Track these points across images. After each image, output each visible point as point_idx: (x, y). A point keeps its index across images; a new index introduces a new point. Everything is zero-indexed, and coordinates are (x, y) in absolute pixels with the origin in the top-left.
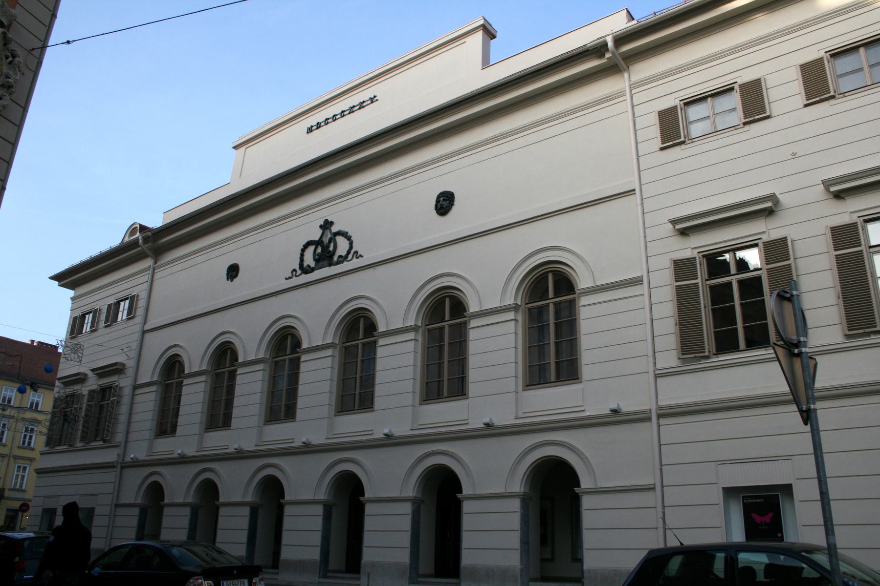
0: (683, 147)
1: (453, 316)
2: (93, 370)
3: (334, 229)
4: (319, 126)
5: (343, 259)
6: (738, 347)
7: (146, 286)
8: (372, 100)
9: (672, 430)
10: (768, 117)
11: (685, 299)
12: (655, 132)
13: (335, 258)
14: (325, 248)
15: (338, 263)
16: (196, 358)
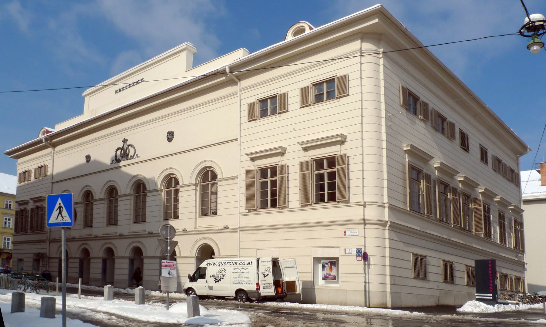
0: (310, 107)
1: (176, 186)
2: (31, 199)
3: (128, 143)
4: (120, 90)
5: (132, 157)
6: (324, 201)
7: (51, 161)
8: (142, 81)
9: (245, 236)
10: (348, 95)
11: (249, 186)
12: (246, 113)
13: (129, 156)
14: (125, 152)
15: (130, 159)
16: (99, 193)
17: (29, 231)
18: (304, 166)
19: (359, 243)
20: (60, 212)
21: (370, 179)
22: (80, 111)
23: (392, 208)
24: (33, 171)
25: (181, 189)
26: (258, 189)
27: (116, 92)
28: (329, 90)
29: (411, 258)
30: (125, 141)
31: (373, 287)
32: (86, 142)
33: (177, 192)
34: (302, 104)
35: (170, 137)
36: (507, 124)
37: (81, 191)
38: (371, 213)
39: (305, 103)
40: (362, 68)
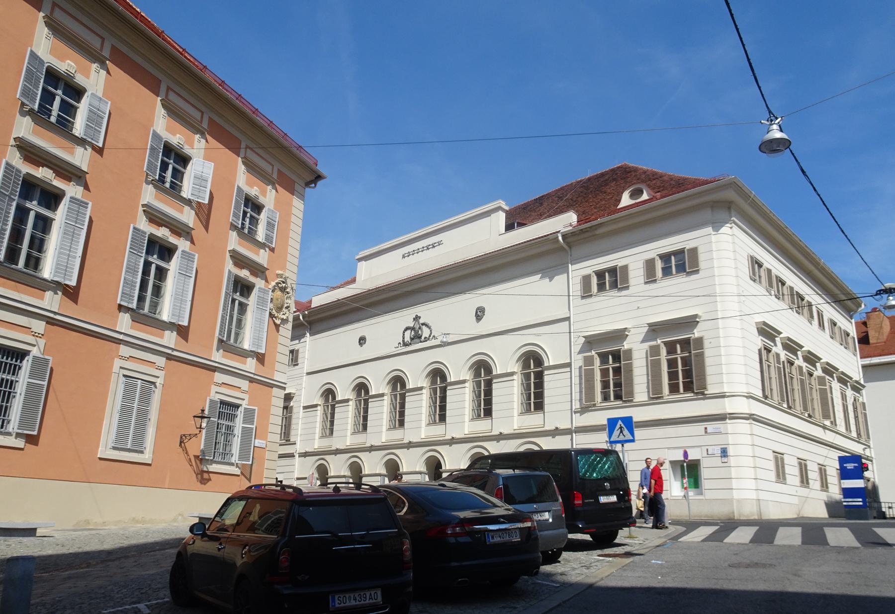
3: (421, 321)
5: (426, 339)
14: (416, 332)
20: (621, 432)
27: (404, 257)
29: (771, 456)
30: (417, 318)
36: (792, 229)
37: (520, 348)
39: (650, 277)
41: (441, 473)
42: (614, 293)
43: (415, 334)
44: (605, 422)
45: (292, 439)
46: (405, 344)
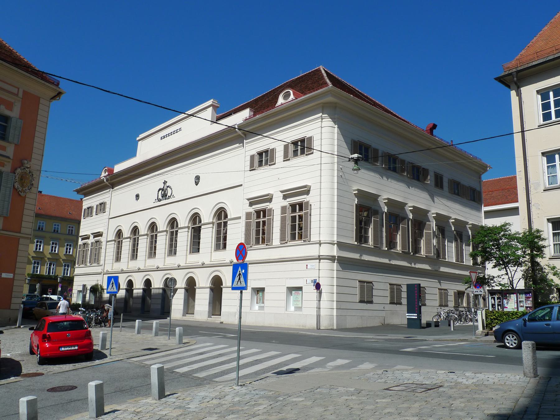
2: (92, 234)
3: (167, 185)
11: (248, 225)
17: (88, 264)
18: (284, 209)
19: (314, 275)
20: (239, 279)
21: (327, 222)
22: (133, 154)
23: (341, 246)
24: (95, 207)
25: (229, 222)
26: (289, 222)
27: (161, 139)
28: (302, 147)
30: (165, 182)
31: (323, 313)
32: (156, 175)
33: (225, 224)
34: (251, 167)
35: (197, 181)
37: (213, 209)
38: (326, 250)
39: (286, 158)
40: (322, 131)
41: (133, 290)
42: (268, 167)
43: (164, 193)
44: (406, 322)
45: (142, 331)
46: (159, 200)
